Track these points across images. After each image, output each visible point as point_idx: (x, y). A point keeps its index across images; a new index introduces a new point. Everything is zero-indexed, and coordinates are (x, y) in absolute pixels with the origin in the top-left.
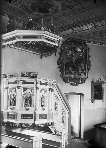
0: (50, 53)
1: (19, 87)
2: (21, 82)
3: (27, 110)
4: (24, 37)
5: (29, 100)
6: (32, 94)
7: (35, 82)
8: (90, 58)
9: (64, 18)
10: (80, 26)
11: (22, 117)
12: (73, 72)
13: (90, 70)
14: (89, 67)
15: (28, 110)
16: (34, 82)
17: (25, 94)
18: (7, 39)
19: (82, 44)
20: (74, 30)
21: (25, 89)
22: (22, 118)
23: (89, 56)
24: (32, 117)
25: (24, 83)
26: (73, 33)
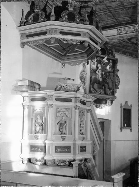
0: (78, 61)
1: (51, 106)
2: (54, 98)
3: (63, 139)
4: (62, 33)
5: (65, 125)
6: (69, 116)
7: (73, 99)
8: (118, 72)
9: (114, 11)
10: (130, 26)
11: (56, 149)
12: (99, 90)
13: (118, 88)
14: (117, 85)
15: (64, 139)
16: (72, 98)
17: (59, 116)
18: (31, 33)
19: (109, 54)
20: (120, 31)
21: (58, 110)
22: (56, 152)
23: (118, 70)
24: (70, 150)
25: (58, 99)
26: (117, 35)
